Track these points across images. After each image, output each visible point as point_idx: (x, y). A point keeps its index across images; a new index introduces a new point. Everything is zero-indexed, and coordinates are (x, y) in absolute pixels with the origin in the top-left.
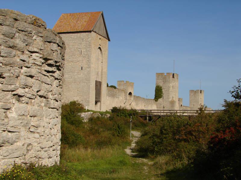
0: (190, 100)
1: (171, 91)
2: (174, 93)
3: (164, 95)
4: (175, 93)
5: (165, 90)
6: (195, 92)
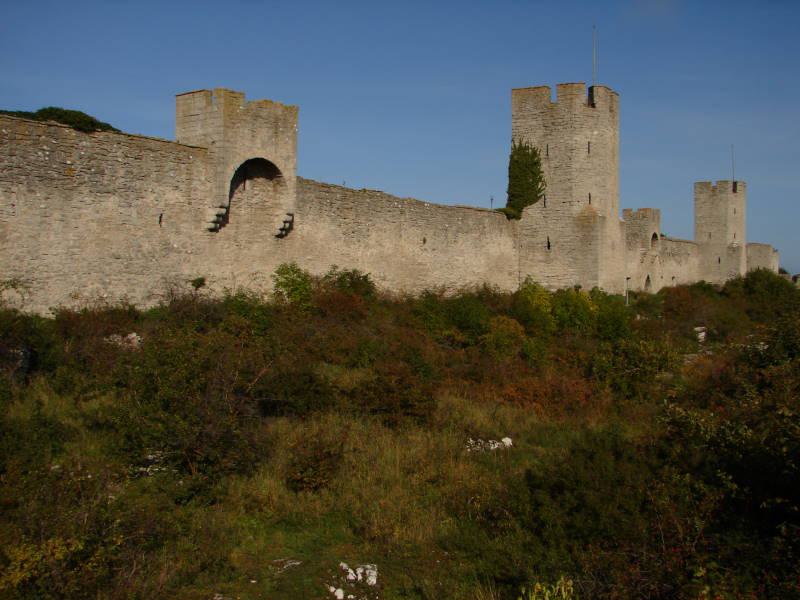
0: (696, 217)
1: (581, 170)
2: (598, 174)
3: (548, 190)
4: (598, 178)
6: (715, 188)
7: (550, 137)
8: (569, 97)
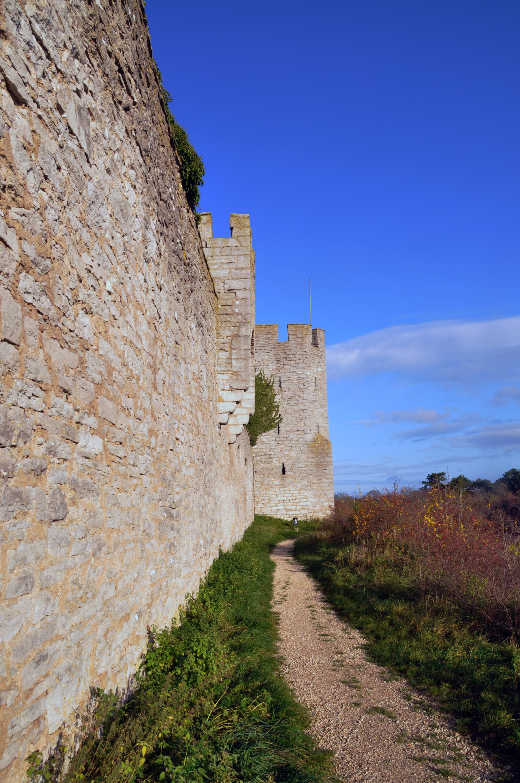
1: (312, 402)
5: (287, 394)
7: (282, 371)
8: (300, 336)
